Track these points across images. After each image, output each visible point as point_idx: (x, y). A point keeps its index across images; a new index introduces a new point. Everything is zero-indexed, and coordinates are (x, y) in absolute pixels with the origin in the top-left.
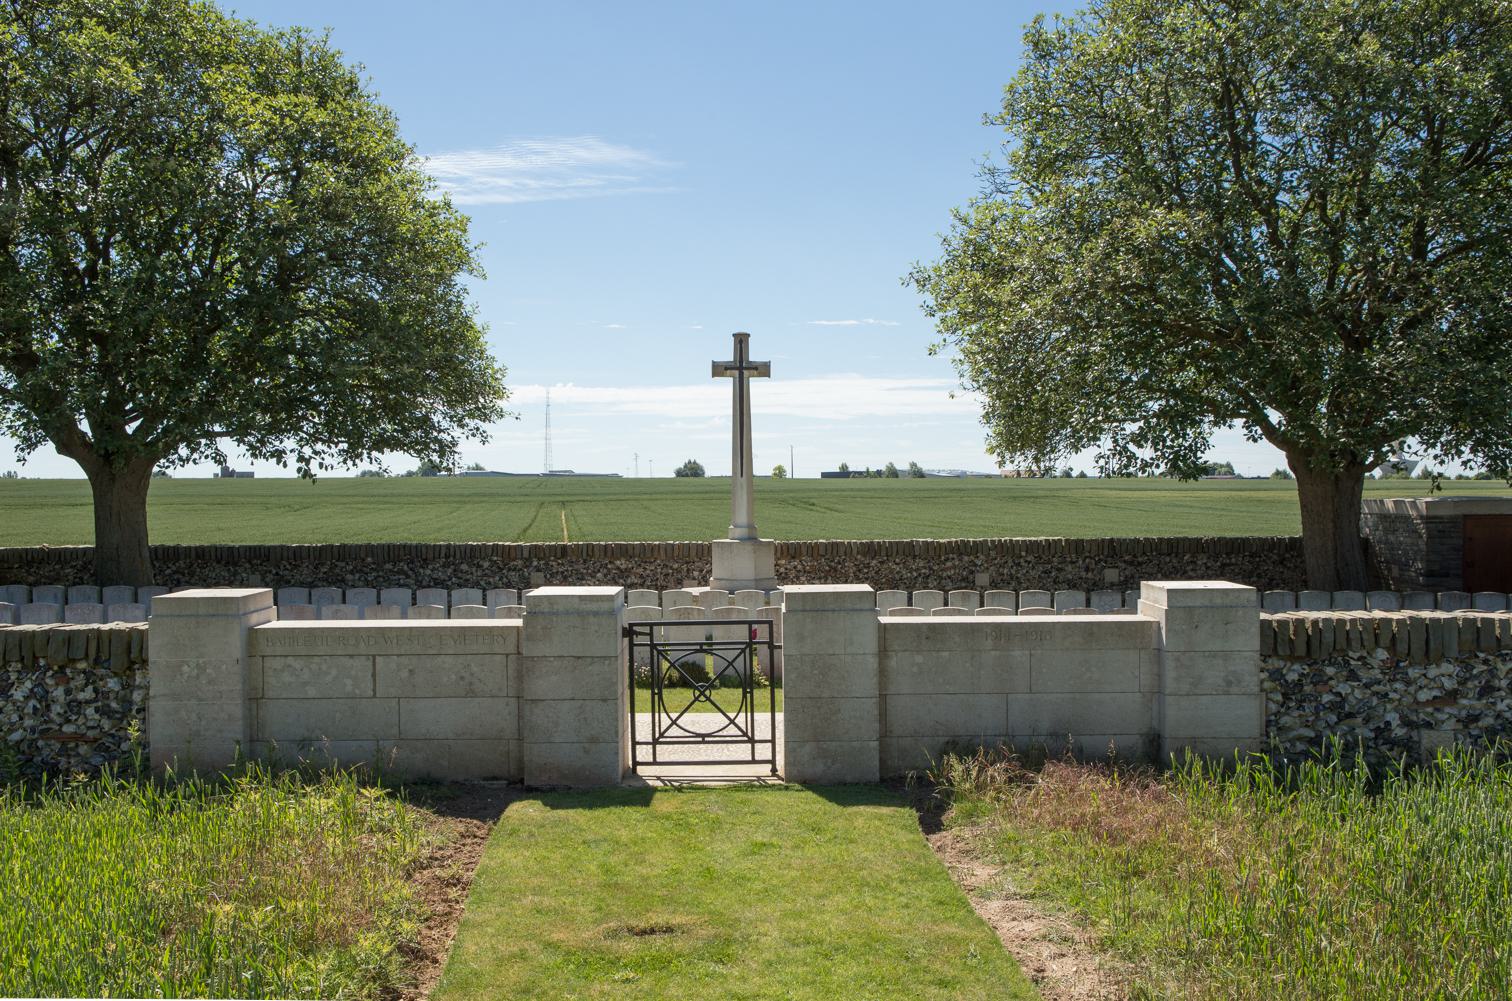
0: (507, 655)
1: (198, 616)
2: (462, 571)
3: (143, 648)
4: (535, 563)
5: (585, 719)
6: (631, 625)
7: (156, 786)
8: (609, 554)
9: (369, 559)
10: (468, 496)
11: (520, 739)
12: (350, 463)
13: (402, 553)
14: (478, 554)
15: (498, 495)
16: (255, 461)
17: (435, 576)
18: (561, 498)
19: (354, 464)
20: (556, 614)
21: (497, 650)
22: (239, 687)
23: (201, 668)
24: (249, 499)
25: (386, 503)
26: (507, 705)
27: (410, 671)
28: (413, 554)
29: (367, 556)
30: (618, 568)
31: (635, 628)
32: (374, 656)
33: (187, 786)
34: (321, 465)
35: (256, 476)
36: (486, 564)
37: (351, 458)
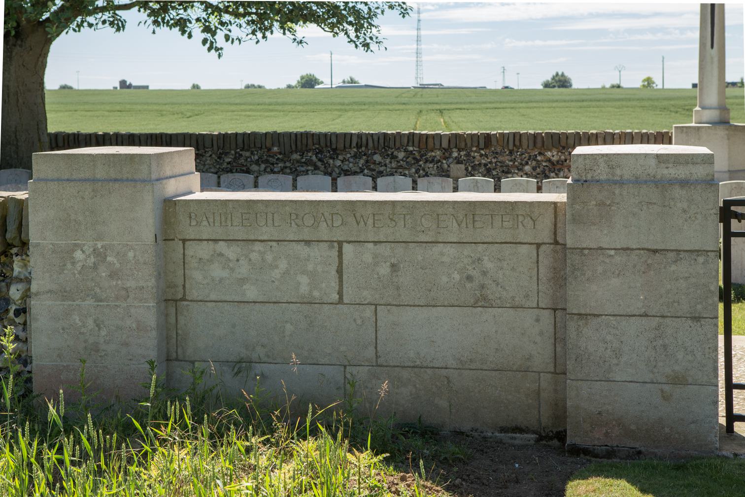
0: (538, 245)
1: (94, 180)
2: (374, 163)
3: (21, 225)
4: (455, 154)
5: (665, 347)
6: (728, 204)
7: (32, 432)
8: (539, 144)
9: (275, 149)
10: (348, 105)
11: (559, 372)
12: (259, 35)
13: (310, 141)
14: (392, 144)
15: (377, 103)
16: (157, 29)
17: (345, 167)
18: (438, 107)
19: (264, 37)
20: (621, 183)
21: (522, 238)
22: (152, 282)
23: (100, 256)
24: (146, 107)
25: (272, 111)
26: (538, 320)
27: (393, 266)
28: (323, 144)
29: (273, 145)
30: (549, 160)
31: (733, 208)
32: (340, 244)
33: (78, 441)
34: (227, 38)
35: (150, 88)
36: (401, 155)
37: (260, 29)
